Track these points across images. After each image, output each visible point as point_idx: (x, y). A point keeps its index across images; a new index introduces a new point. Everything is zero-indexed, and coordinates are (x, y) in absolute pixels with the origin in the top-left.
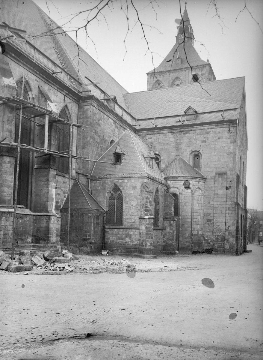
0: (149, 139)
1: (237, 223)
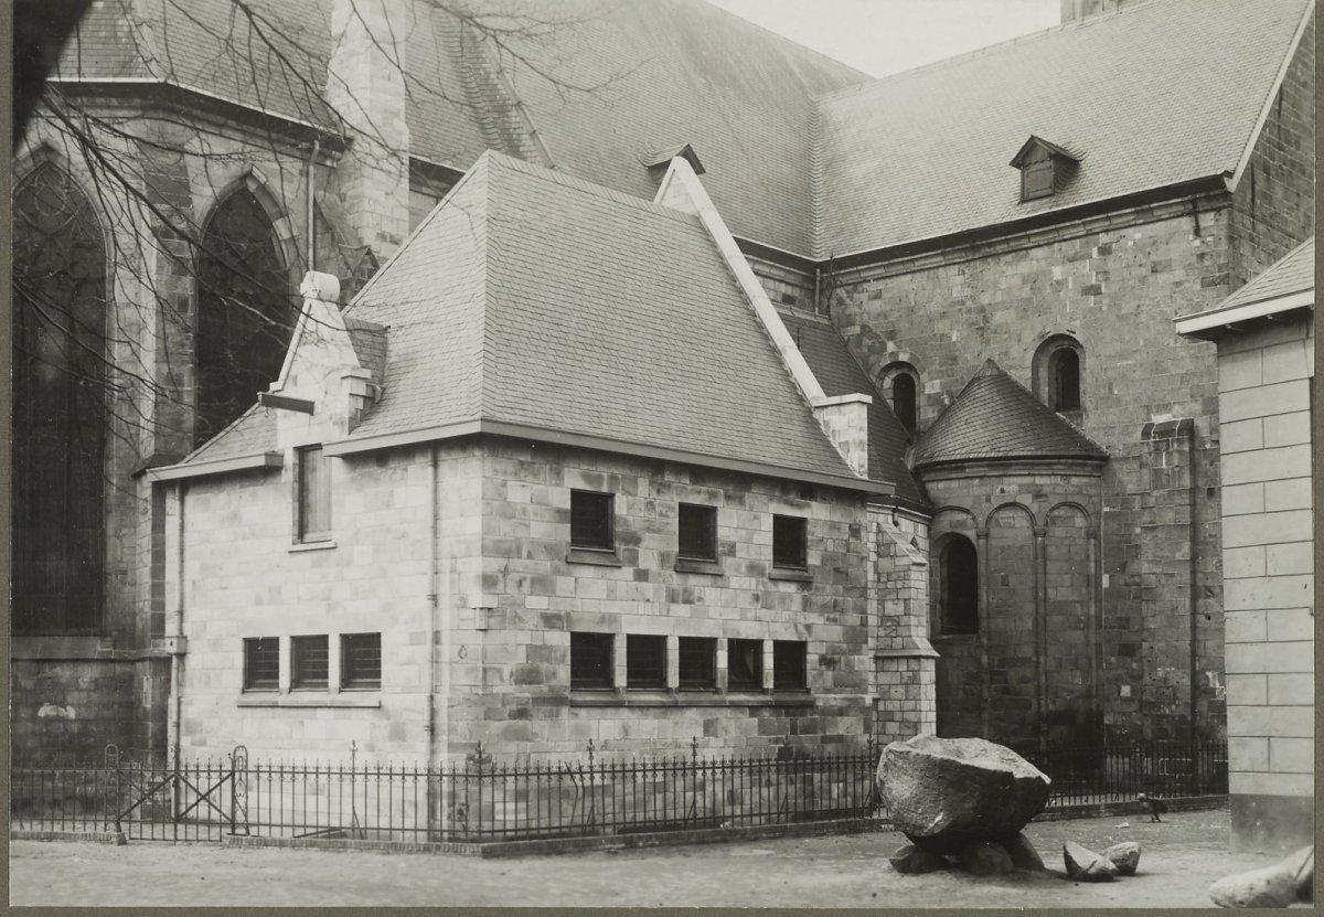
0: (870, 299)
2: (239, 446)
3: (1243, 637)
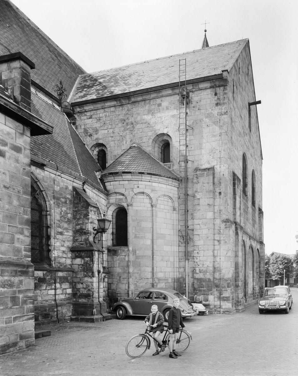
1: (236, 256)
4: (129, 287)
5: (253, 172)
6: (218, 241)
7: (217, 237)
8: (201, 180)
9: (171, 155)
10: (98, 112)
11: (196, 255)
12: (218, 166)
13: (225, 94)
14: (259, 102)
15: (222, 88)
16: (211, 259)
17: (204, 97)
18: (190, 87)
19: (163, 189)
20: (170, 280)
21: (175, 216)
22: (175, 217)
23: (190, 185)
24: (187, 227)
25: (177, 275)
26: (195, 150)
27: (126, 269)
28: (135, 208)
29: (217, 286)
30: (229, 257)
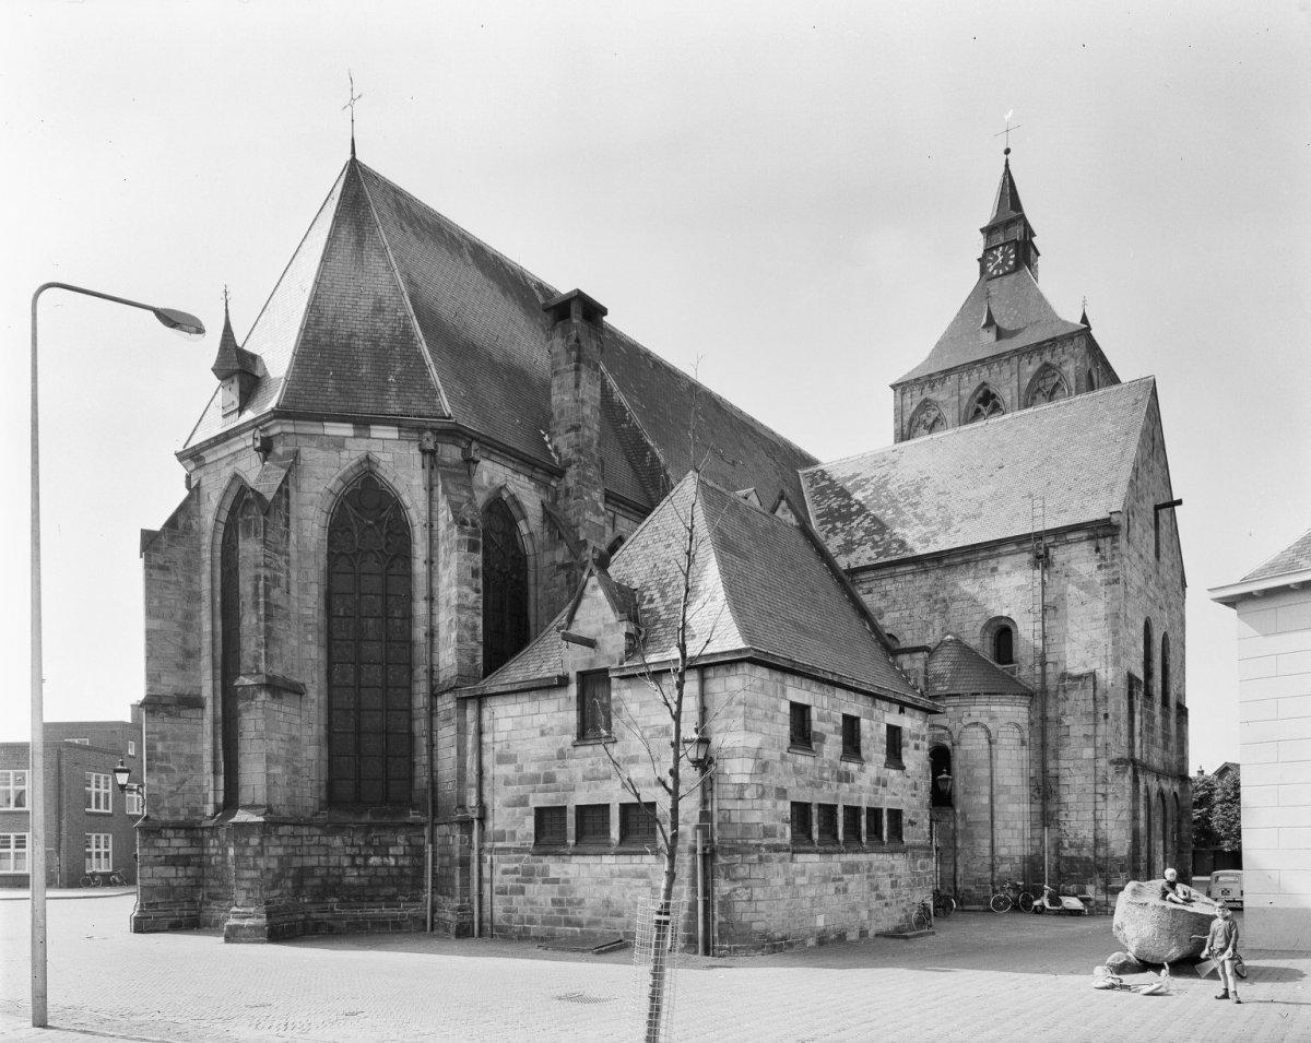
1: (1135, 818)
2: (517, 671)
3: (1250, 826)
4: (955, 870)
5: (1165, 638)
6: (1103, 795)
7: (1101, 790)
8: (1073, 695)
9: (1014, 650)
10: (884, 583)
11: (1063, 818)
12: (1103, 670)
13: (1115, 548)
14: (1179, 502)
15: (1109, 539)
16: (1091, 826)
17: (1079, 560)
18: (1050, 540)
19: (1009, 714)
20: (1017, 860)
21: (1025, 753)
22: (1024, 755)
23: (1051, 702)
24: (1044, 770)
25: (1028, 851)
26: (1059, 644)
27: (951, 842)
28: (963, 748)
29: (1101, 870)
30: (1123, 821)
